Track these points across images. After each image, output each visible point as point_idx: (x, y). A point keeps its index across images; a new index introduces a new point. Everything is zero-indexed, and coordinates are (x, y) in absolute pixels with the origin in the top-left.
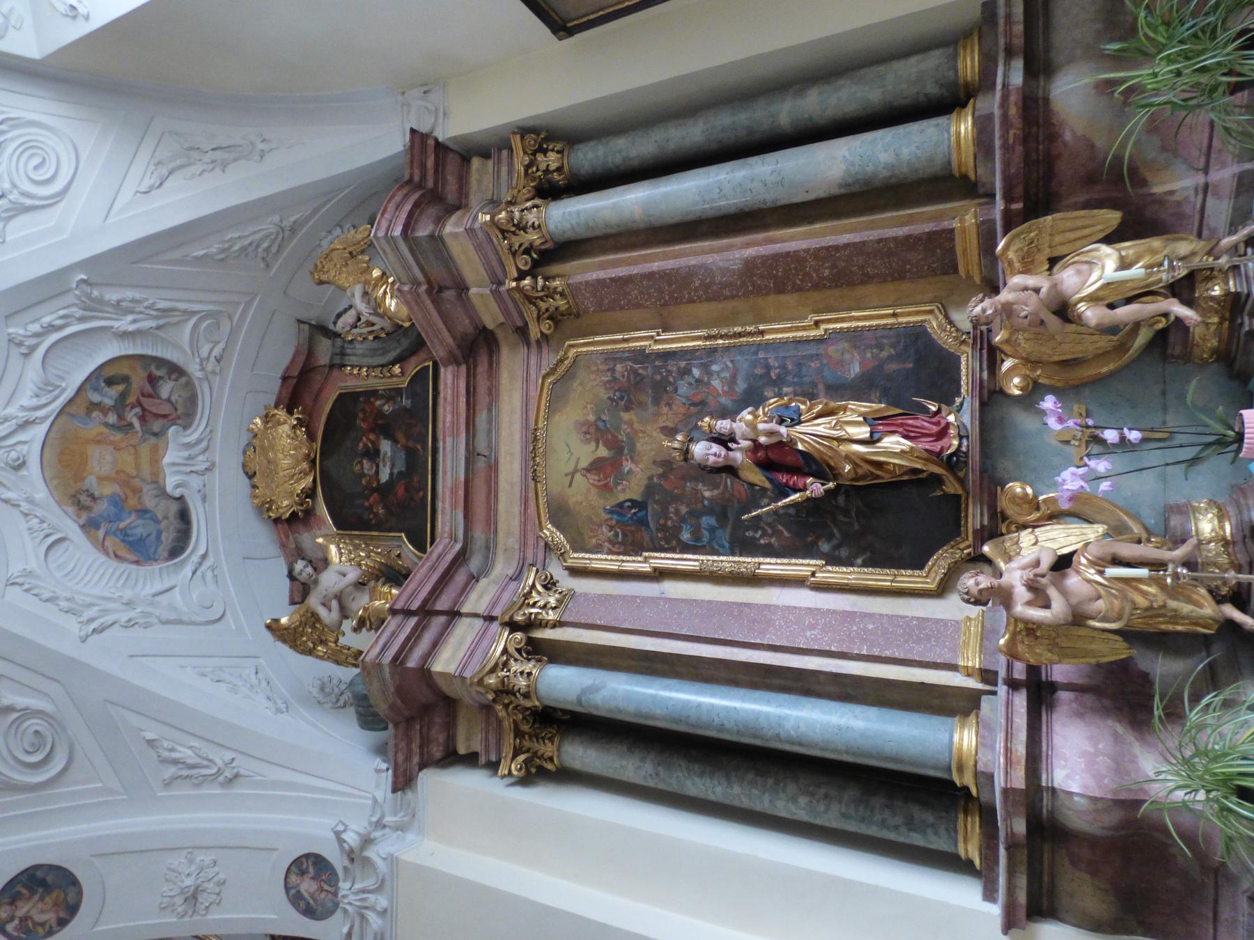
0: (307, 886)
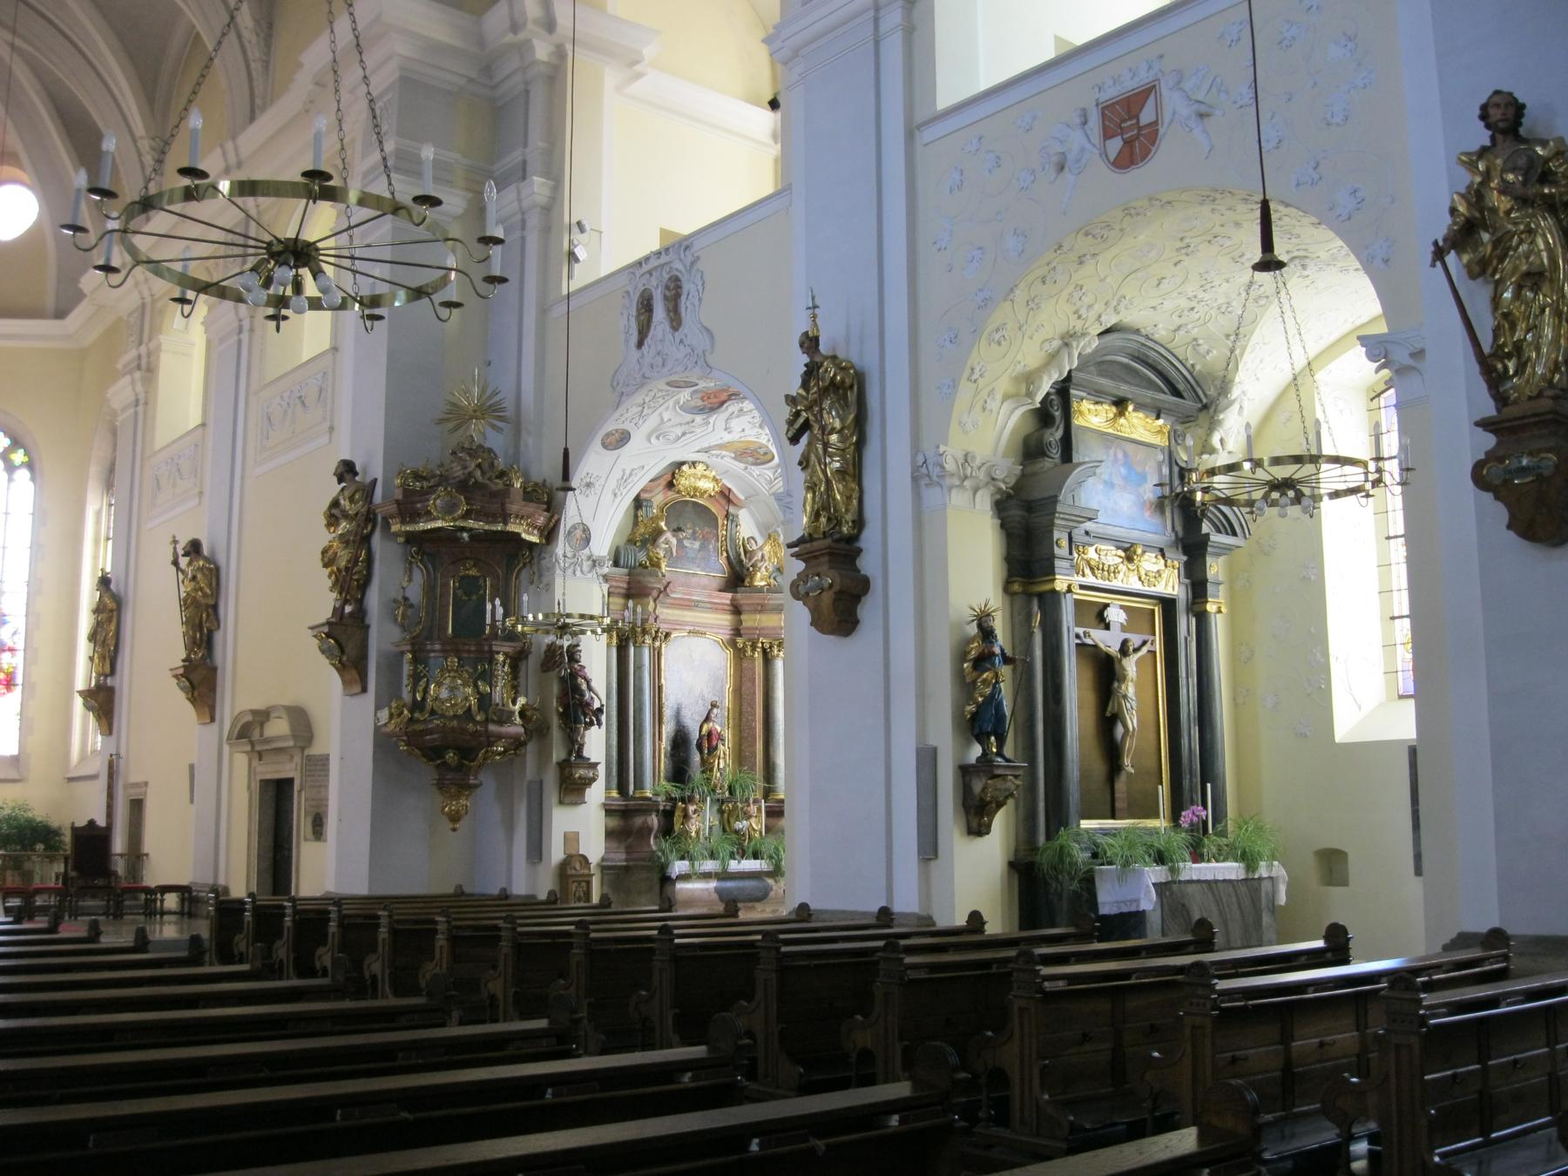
0: (579, 533)
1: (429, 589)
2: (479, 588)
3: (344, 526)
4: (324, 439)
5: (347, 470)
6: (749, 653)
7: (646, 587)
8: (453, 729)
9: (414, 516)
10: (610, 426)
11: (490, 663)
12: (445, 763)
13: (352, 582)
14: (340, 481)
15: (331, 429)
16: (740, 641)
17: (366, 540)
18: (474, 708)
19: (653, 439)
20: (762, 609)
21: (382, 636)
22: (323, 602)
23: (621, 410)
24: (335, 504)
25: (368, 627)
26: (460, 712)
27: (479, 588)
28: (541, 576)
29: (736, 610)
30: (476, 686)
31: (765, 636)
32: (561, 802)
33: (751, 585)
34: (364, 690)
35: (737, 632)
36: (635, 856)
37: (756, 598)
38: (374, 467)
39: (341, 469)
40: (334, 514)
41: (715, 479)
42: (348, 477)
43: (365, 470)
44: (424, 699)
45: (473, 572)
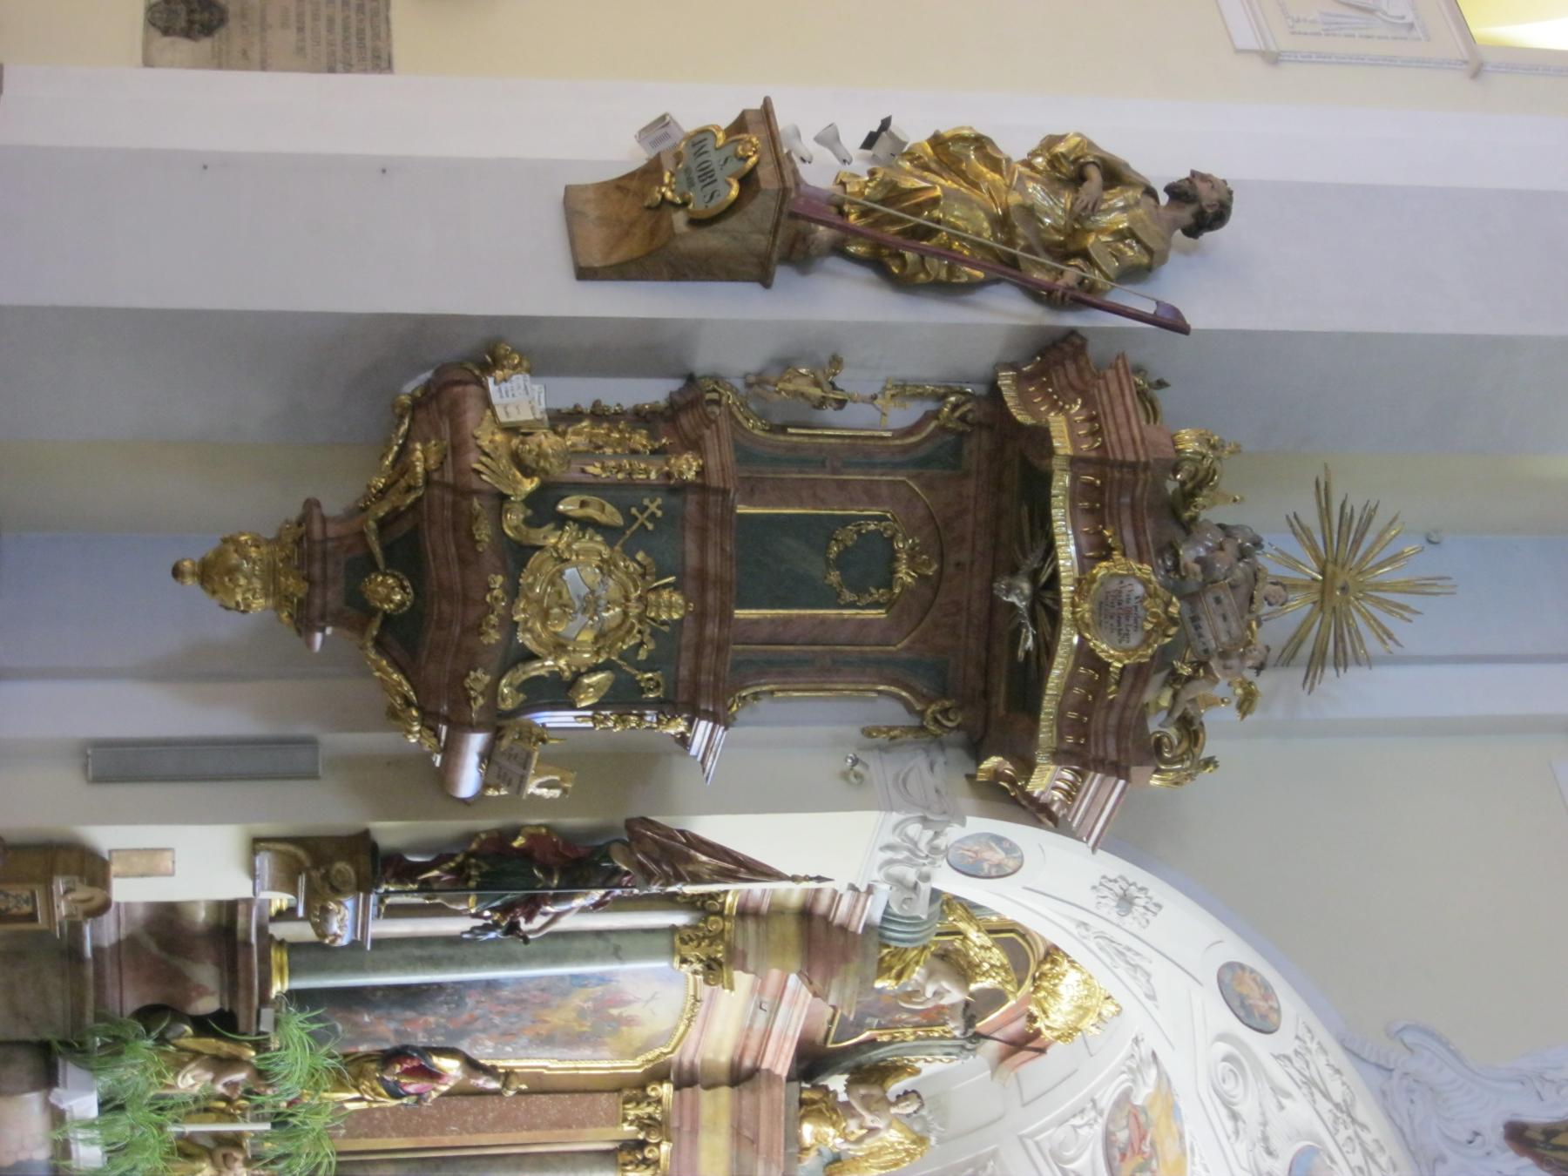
0: (998, 855)
1: (862, 452)
2: (861, 590)
3: (1053, 207)
4: (1247, 38)
5: (1200, 208)
6: (632, 1112)
7: (829, 973)
8: (478, 629)
9: (1096, 504)
10: (1290, 1005)
11: (659, 705)
12: (370, 566)
13: (894, 235)
14: (1172, 190)
15: (1273, 59)
16: (666, 1090)
17: (1005, 268)
18: (536, 669)
19: (1223, 1048)
20: (743, 1136)
21: (732, 324)
22: (827, 138)
23: (1338, 1056)
24: (1114, 174)
25: (765, 279)
26: (524, 638)
27: (861, 590)
28: (883, 749)
29: (741, 1077)
30: (594, 669)
31: (675, 1152)
32: (257, 844)
33: (802, 1118)
34: (584, 274)
35: (687, 1079)
36: (110, 971)
37: (770, 1132)
38: (1211, 291)
39: (1207, 196)
40: (1081, 171)
41: (1068, 1035)
42: (1186, 214)
43: (1186, 252)
44: (562, 520)
45: (905, 575)
